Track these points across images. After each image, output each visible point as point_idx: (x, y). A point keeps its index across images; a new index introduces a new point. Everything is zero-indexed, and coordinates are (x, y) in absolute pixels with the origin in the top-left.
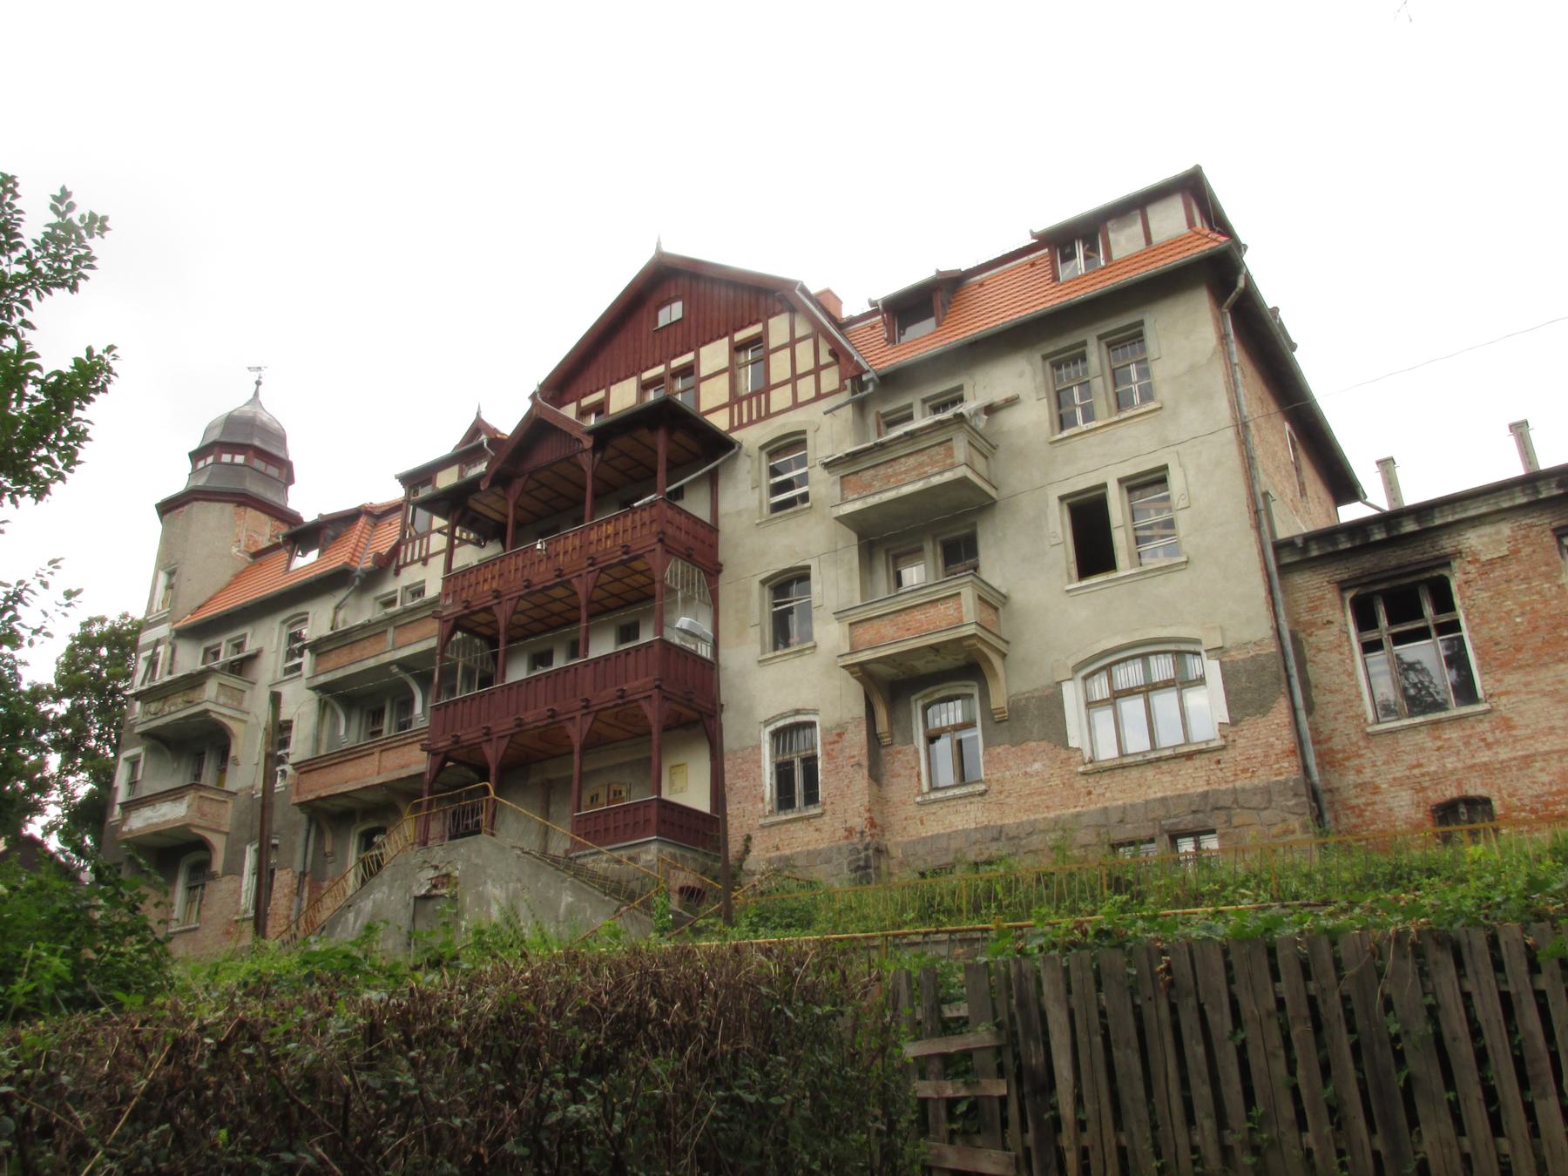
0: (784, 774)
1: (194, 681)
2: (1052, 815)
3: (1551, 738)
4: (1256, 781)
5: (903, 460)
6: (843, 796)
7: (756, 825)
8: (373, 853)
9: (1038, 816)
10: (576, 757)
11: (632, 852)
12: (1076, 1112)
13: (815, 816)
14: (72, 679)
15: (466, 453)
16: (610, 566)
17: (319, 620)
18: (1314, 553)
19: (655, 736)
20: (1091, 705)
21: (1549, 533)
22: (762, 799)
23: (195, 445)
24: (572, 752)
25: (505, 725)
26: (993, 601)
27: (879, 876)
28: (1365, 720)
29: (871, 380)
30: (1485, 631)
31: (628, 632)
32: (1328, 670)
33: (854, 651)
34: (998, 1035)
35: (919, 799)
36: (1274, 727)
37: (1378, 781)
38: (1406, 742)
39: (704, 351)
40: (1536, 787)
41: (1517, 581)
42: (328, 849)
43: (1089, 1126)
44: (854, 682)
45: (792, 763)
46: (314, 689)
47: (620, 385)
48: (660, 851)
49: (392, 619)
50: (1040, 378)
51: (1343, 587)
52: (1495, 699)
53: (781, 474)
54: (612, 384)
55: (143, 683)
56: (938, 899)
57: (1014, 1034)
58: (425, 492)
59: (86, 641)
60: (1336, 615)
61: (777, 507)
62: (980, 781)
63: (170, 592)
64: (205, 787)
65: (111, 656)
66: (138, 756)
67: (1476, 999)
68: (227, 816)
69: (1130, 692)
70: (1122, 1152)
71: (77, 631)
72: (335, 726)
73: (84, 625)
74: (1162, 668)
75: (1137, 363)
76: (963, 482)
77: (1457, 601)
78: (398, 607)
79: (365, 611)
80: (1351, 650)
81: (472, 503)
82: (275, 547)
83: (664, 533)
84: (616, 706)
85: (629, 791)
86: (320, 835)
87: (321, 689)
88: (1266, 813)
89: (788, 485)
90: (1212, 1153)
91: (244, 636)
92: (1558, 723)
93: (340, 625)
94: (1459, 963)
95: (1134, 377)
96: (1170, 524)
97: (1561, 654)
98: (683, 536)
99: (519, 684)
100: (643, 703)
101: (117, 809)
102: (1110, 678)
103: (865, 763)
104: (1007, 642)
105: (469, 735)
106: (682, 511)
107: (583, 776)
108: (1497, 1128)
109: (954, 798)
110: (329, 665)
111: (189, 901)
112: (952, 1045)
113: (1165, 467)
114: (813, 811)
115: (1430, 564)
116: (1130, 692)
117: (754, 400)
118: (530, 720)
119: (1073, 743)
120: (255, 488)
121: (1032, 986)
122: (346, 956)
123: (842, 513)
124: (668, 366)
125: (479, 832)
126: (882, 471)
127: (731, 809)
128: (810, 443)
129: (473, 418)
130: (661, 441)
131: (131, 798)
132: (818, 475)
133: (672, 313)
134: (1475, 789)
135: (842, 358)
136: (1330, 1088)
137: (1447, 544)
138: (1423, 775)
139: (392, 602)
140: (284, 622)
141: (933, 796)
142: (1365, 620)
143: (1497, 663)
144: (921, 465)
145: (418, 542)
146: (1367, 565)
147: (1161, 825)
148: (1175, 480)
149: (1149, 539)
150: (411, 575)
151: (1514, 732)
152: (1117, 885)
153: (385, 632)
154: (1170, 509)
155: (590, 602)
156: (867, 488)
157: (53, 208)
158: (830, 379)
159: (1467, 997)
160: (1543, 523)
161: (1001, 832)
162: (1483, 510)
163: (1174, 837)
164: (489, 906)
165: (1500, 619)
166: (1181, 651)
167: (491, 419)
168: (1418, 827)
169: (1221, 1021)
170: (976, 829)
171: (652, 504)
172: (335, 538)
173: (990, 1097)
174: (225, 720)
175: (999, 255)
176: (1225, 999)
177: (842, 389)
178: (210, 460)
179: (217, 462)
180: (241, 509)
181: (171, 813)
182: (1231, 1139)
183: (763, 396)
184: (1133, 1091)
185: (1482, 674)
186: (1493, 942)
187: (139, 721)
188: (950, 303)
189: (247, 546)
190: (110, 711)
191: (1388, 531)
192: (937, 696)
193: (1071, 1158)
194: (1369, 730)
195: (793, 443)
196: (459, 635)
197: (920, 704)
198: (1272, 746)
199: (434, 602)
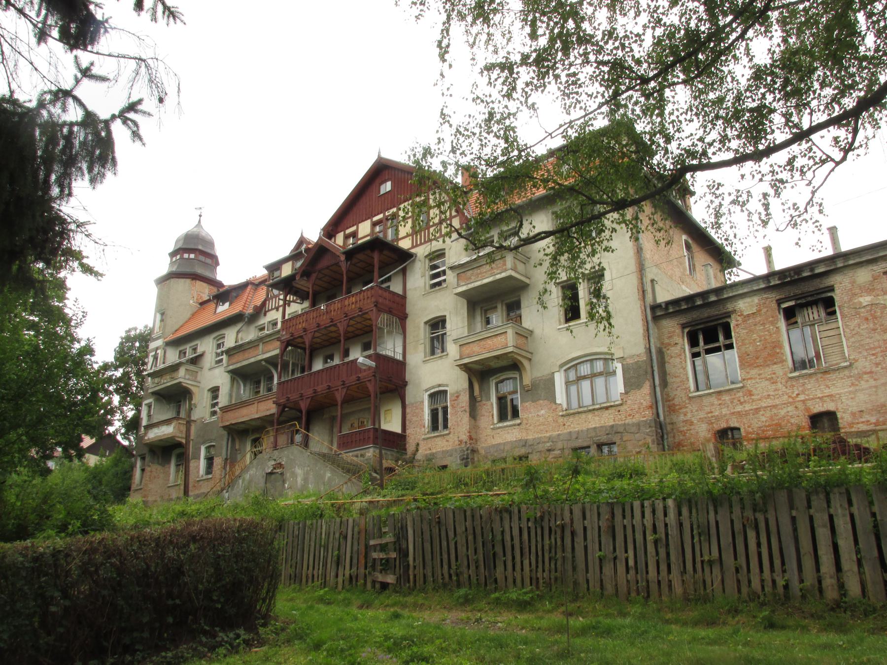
0: (434, 414)
1: (174, 368)
2: (548, 435)
4: (634, 420)
6: (458, 425)
10: (339, 407)
11: (363, 452)
14: (124, 357)
15: (294, 256)
16: (354, 317)
17: (231, 338)
18: (671, 310)
20: (568, 383)
23: (171, 248)
24: (337, 405)
25: (309, 392)
26: (525, 335)
27: (473, 463)
30: (743, 349)
32: (674, 366)
36: (643, 396)
38: (706, 401)
42: (237, 447)
45: (437, 409)
46: (229, 372)
49: (261, 339)
51: (683, 326)
59: (128, 339)
60: (679, 340)
61: (434, 286)
65: (141, 346)
69: (584, 378)
70: (424, 575)
71: (124, 335)
72: (239, 388)
73: (127, 332)
74: (599, 366)
77: (733, 334)
79: (250, 334)
80: (685, 357)
82: (208, 301)
86: (233, 441)
87: (232, 372)
88: (637, 435)
90: (446, 576)
92: (772, 393)
94: (511, 518)
99: (319, 371)
101: (143, 429)
102: (576, 370)
103: (468, 410)
105: (294, 397)
109: (507, 426)
110: (234, 361)
112: (384, 541)
114: (446, 432)
116: (584, 378)
119: (558, 402)
120: (200, 271)
126: (475, 271)
127: (408, 432)
128: (447, 255)
129: (299, 236)
130: (376, 256)
133: (387, 187)
134: (734, 424)
137: (730, 307)
139: (262, 329)
142: (694, 343)
146: (695, 316)
155: (346, 332)
156: (468, 280)
159: (511, 528)
162: (745, 290)
165: (750, 343)
166: (608, 359)
168: (708, 441)
171: (372, 288)
172: (236, 297)
178: (178, 257)
179: (182, 258)
181: (166, 431)
184: (428, 556)
185: (741, 369)
186: (519, 512)
191: (703, 300)
193: (411, 577)
195: (440, 254)
196: (290, 348)
197: (494, 381)
199: (278, 332)
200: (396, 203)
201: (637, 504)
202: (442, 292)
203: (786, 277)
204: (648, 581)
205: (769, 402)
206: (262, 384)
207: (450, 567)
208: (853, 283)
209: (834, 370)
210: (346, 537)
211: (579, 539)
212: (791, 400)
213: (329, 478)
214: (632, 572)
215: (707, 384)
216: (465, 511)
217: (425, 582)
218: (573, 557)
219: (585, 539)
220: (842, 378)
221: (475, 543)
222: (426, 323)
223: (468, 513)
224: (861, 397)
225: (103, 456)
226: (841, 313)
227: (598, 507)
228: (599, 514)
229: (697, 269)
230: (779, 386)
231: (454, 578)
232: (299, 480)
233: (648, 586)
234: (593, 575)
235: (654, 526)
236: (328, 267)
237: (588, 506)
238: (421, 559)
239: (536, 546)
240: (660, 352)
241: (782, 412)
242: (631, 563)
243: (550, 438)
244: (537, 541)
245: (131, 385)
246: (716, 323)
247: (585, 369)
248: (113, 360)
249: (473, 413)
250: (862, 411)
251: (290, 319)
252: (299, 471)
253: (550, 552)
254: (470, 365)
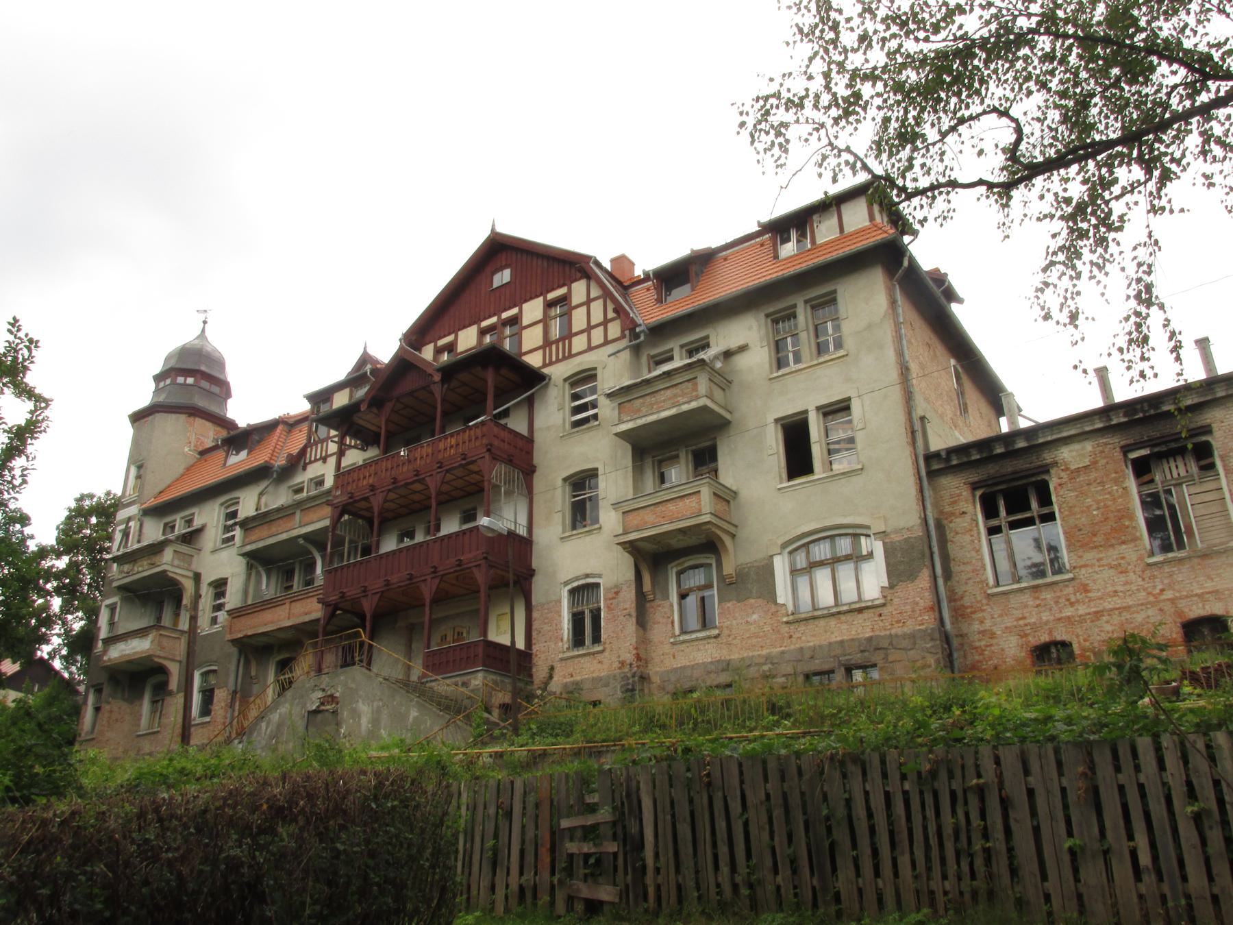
0: (577, 620)
1: (156, 549)
2: (764, 652)
3: (1114, 599)
4: (905, 629)
5: (662, 392)
6: (618, 638)
7: (557, 659)
8: (287, 676)
9: (756, 653)
10: (427, 609)
11: (465, 678)
12: (655, 863)
13: (598, 652)
14: (69, 540)
15: (354, 381)
17: (248, 503)
18: (955, 462)
19: (482, 594)
20: (794, 572)
21: (1118, 449)
22: (562, 640)
23: (158, 369)
24: (424, 605)
25: (377, 585)
26: (726, 497)
28: (987, 584)
29: (643, 331)
31: (469, 516)
32: (962, 547)
34: (614, 813)
35: (672, 640)
36: (919, 591)
37: (994, 629)
38: (1015, 601)
39: (525, 306)
40: (1103, 634)
41: (1095, 485)
42: (253, 673)
43: (662, 871)
44: (627, 554)
45: (583, 613)
46: (243, 555)
47: (465, 331)
48: (485, 678)
49: (298, 505)
50: (763, 332)
51: (974, 487)
52: (1078, 570)
53: (582, 398)
54: (460, 330)
55: (118, 550)
56: (657, 717)
57: (623, 813)
58: (324, 409)
59: (79, 513)
60: (968, 507)
62: (715, 627)
63: (139, 480)
64: (165, 628)
66: (115, 603)
67: (871, 795)
70: (679, 887)
71: (73, 505)
72: (259, 582)
74: (844, 546)
75: (832, 320)
76: (704, 409)
77: (1054, 498)
78: (305, 494)
79: (281, 498)
80: (979, 533)
81: (356, 419)
83: (491, 445)
84: (455, 571)
85: (468, 633)
86: (247, 664)
88: (911, 653)
89: (583, 408)
90: (727, 888)
91: (193, 514)
92: (1120, 588)
93: (263, 507)
94: (864, 774)
95: (830, 331)
96: (851, 440)
97: (1123, 538)
98: (506, 446)
100: (475, 571)
101: (100, 643)
102: (808, 553)
103: (634, 614)
104: (736, 526)
105: (353, 592)
106: (505, 427)
107: (432, 622)
108: (877, 874)
109: (697, 639)
110: (254, 538)
111: (153, 711)
112: (590, 820)
113: (849, 399)
114: (598, 648)
115: (1035, 471)
116: (821, 564)
117: (560, 344)
118: (395, 581)
119: (780, 600)
120: (201, 403)
121: (634, 784)
122: (161, 775)
123: (619, 431)
124: (499, 317)
125: (354, 664)
126: (648, 399)
127: (535, 648)
128: (599, 377)
129: (361, 352)
130: (490, 377)
131: (111, 635)
132: (603, 402)
133: (504, 277)
134: (1060, 636)
135: (622, 315)
136: (792, 849)
137: (1048, 457)
138: (1026, 625)
139: (299, 490)
140: (222, 504)
141: (681, 638)
142: (990, 511)
143: (1079, 544)
144: (675, 396)
145: (319, 445)
146: (992, 471)
147: (839, 661)
148: (856, 406)
149: (838, 451)
150: (314, 470)
151: (1089, 595)
152: (773, 709)
153: (294, 513)
154: (852, 429)
155: (439, 493)
157: (9, 331)
158: (614, 330)
159: (867, 793)
160: (1114, 442)
161: (728, 664)
162: (1073, 432)
163: (849, 670)
164: (360, 717)
165: (1083, 512)
166: (856, 533)
167: (372, 352)
169: (735, 807)
170: (711, 663)
171: (483, 423)
172: (259, 442)
173: (608, 853)
175: (742, 235)
176: (738, 793)
177: (623, 336)
178: (168, 381)
179: (174, 383)
180: (192, 418)
182: (738, 879)
183: (567, 341)
184: (686, 849)
185: (1069, 552)
186: (883, 762)
187: (116, 577)
188: (702, 272)
189: (196, 446)
190: (96, 566)
191: (1006, 447)
192: (687, 564)
193: (651, 890)
194: (989, 591)
195: (587, 377)
196: (346, 517)
197: (675, 570)
198: (917, 604)
199: (329, 492)
200: (519, 301)
201: (1144, 743)
202: (592, 433)
203: (1136, 412)
204: (1188, 897)
205: (1118, 602)
206: (296, 578)
207: (733, 869)
209: (1219, 553)
210: (509, 814)
211: (1020, 812)
212: (1151, 599)
213: (416, 719)
214: (1149, 879)
215: (1013, 575)
216: (764, 762)
217: (680, 900)
218: (1010, 850)
219: (1034, 813)
221: (788, 821)
222: (565, 480)
223: (772, 765)
225: (29, 691)
226: (1225, 467)
227: (1057, 751)
228: (1059, 764)
229: (970, 410)
230: (1132, 576)
231: (745, 892)
232: (365, 722)
233: (1190, 907)
234: (1059, 882)
235: (1189, 784)
236: (411, 394)
237: (1033, 749)
238: (671, 854)
239: (925, 828)
240: (940, 526)
241: (1139, 618)
242: (1145, 859)
243: (768, 658)
244: (924, 818)
245: (81, 583)
246: (1024, 481)
247: (822, 551)
248: (54, 543)
251: (349, 472)
252: (364, 709)
253: (957, 838)
254: (639, 544)
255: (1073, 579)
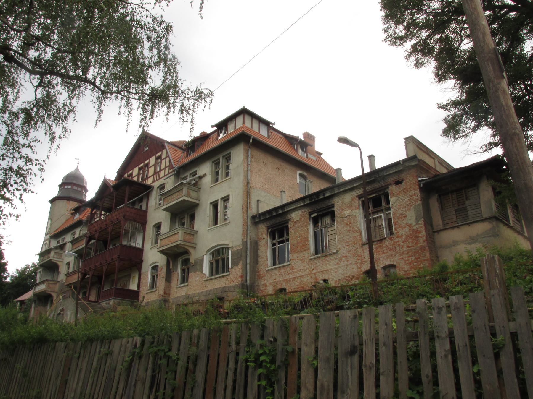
9: (195, 292)
18: (262, 219)
23: (60, 182)
25: (93, 267)
32: (262, 252)
33: (160, 247)
48: (114, 301)
51: (268, 228)
68: (57, 287)
76: (184, 201)
80: (267, 246)
88: (234, 293)
92: (302, 268)
110: (75, 247)
119: (204, 273)
120: (73, 195)
127: (141, 289)
130: (127, 189)
137: (289, 216)
140: (72, 234)
142: (273, 238)
144: (178, 195)
151: (294, 271)
162: (295, 207)
165: (295, 238)
174: (56, 262)
180: (68, 202)
208: (343, 202)
212: (310, 273)
220: (333, 260)
224: (340, 271)
241: (305, 280)
246: (282, 226)
249: (168, 278)
250: (339, 280)
255: (289, 265)
